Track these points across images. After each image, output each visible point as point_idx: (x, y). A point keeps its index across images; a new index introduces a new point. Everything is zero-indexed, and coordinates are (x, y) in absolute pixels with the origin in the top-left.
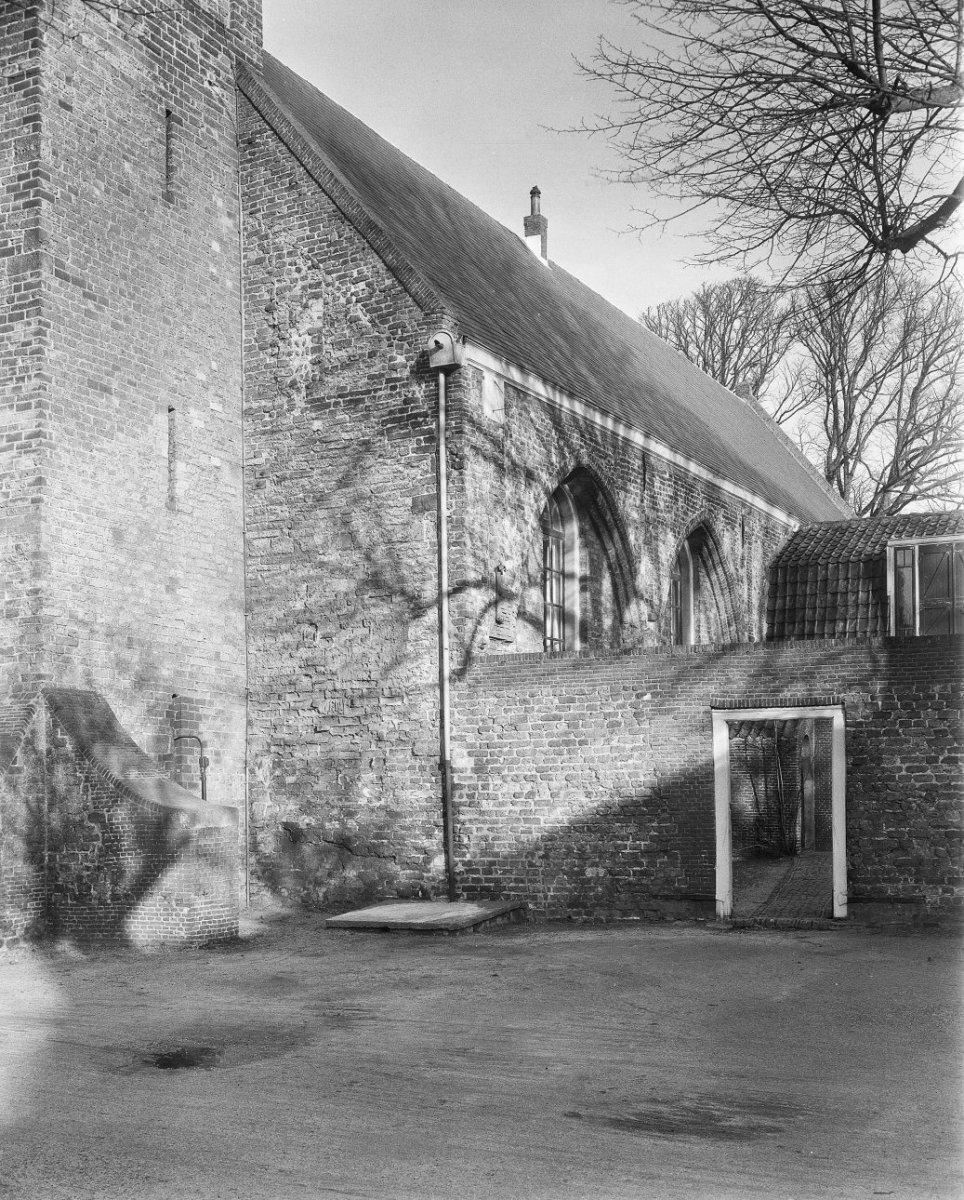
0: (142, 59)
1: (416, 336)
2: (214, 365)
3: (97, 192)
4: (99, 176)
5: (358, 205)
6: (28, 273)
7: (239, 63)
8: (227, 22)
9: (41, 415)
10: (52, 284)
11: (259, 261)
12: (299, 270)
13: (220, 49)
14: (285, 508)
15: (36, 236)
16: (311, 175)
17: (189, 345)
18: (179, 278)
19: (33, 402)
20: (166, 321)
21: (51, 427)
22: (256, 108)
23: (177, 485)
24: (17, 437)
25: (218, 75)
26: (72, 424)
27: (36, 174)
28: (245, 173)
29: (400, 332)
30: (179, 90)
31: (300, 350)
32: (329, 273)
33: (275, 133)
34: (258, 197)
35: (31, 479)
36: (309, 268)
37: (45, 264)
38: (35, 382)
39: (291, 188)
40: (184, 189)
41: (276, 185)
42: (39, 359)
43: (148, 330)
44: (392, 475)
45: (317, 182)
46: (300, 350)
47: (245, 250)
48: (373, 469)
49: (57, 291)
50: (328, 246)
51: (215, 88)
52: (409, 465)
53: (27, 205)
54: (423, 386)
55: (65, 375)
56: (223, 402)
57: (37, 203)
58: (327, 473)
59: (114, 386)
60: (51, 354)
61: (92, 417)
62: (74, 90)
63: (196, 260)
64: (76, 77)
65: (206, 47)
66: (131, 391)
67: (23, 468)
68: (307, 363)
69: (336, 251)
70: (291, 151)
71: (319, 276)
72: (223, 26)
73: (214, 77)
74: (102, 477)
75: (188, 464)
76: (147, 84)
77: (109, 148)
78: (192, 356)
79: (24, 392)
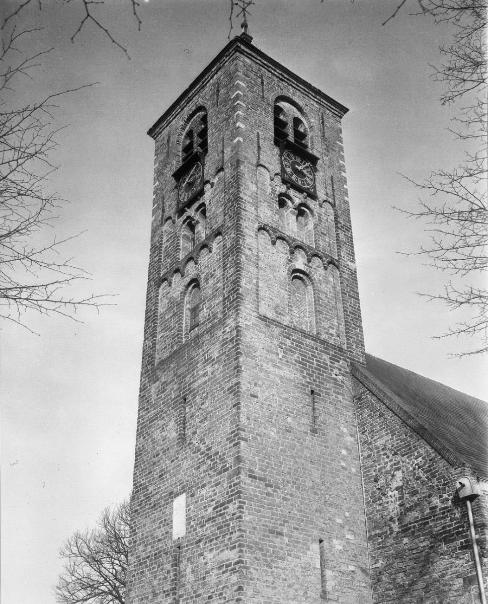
0: (297, 370)
1: (452, 481)
2: (347, 514)
3: (272, 433)
4: (274, 426)
5: (413, 418)
6: (235, 478)
7: (351, 364)
8: (345, 347)
9: (241, 551)
10: (247, 482)
11: (369, 456)
12: (388, 457)
13: (340, 359)
14: (394, 591)
15: (238, 459)
16: (389, 408)
17: (331, 505)
18: (323, 470)
19: (237, 544)
20: (316, 493)
21: (247, 557)
22: (361, 382)
23: (327, 584)
24: (229, 565)
25: (340, 370)
26: (259, 554)
27: (238, 430)
28: (358, 414)
29: (443, 481)
30: (318, 380)
31: (393, 500)
32: (403, 456)
33: (371, 392)
34: (365, 424)
35: (236, 588)
36: (393, 455)
37: (243, 472)
38: (238, 533)
39: (380, 416)
40: (323, 426)
41: (373, 417)
42: (239, 521)
43: (305, 499)
44: (449, 566)
45: (392, 411)
46: (393, 500)
47: (362, 451)
48: (438, 563)
49: (249, 485)
50: (401, 442)
51: (339, 377)
52: (457, 558)
53: (234, 445)
54: (460, 509)
55: (255, 528)
56: (354, 533)
57: (238, 443)
58: (413, 568)
59: (285, 531)
60: (246, 518)
61: (272, 549)
62: (259, 388)
63: (332, 460)
64: (260, 383)
65: (333, 359)
66: (296, 534)
67: (232, 582)
68: (397, 506)
69: (405, 444)
70: (379, 399)
71: (398, 458)
72: (342, 349)
73: (338, 372)
74: (279, 582)
75: (333, 571)
76: (300, 380)
77: (279, 412)
78: (333, 510)
79: (233, 540)
